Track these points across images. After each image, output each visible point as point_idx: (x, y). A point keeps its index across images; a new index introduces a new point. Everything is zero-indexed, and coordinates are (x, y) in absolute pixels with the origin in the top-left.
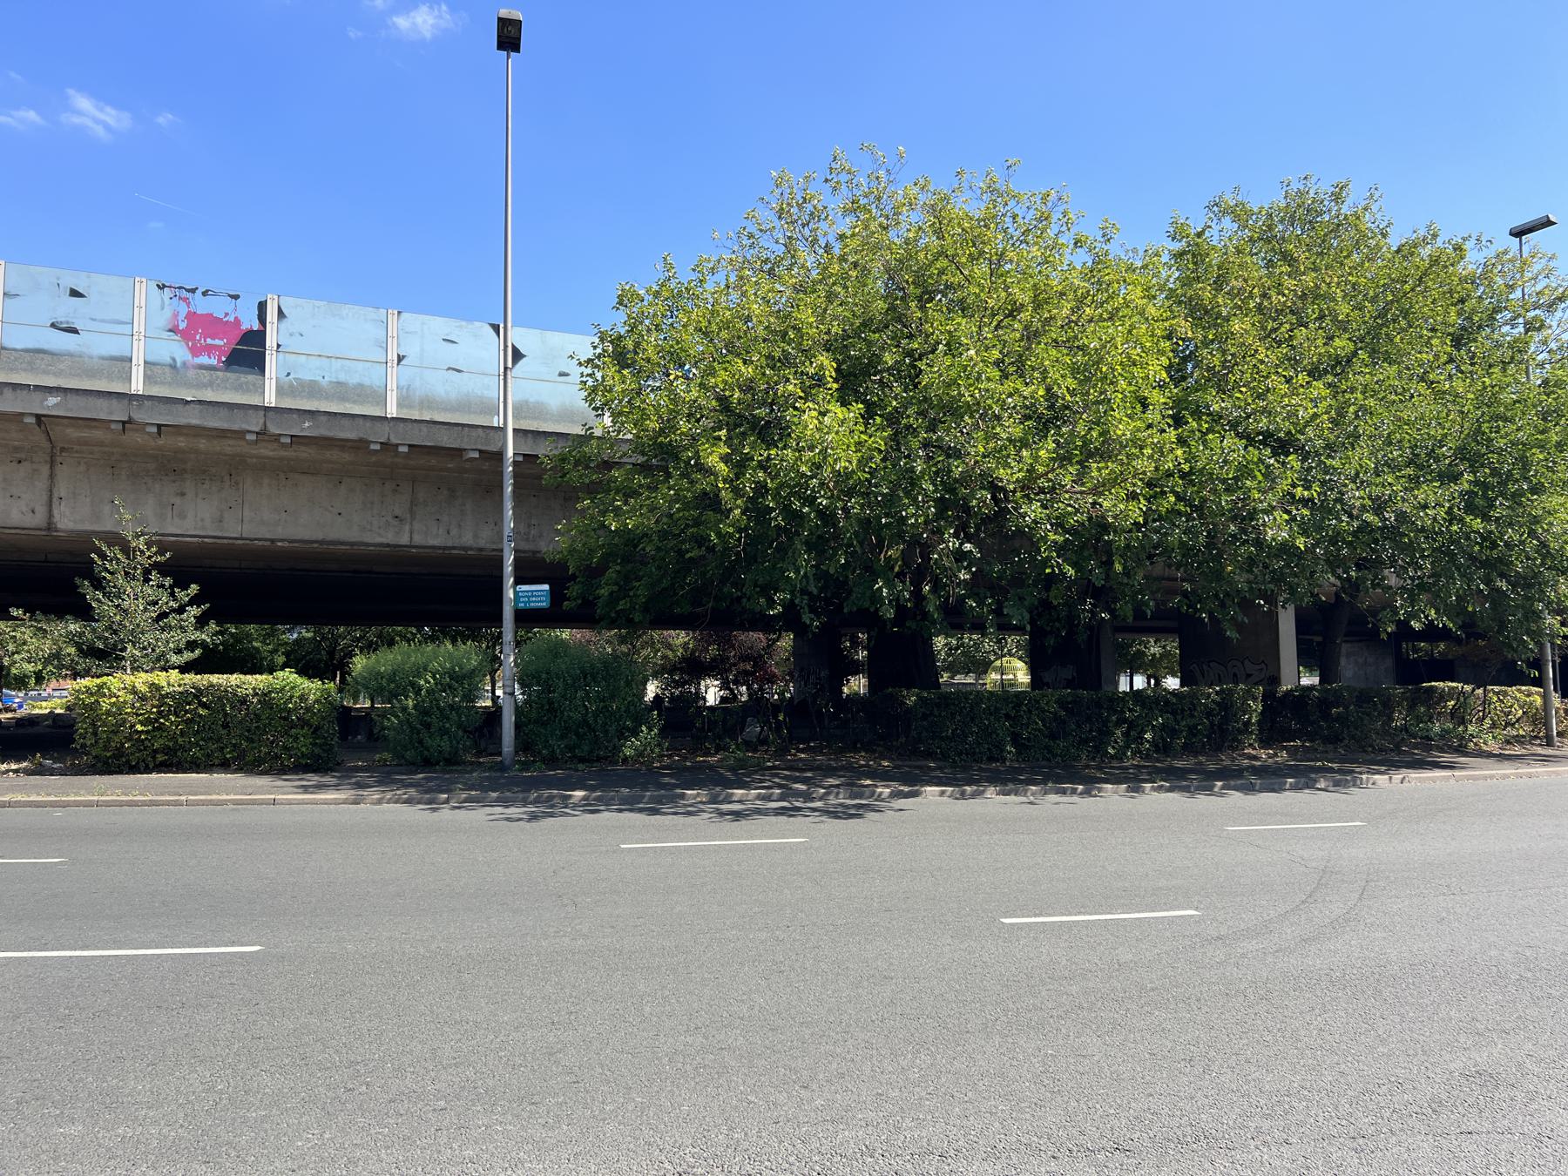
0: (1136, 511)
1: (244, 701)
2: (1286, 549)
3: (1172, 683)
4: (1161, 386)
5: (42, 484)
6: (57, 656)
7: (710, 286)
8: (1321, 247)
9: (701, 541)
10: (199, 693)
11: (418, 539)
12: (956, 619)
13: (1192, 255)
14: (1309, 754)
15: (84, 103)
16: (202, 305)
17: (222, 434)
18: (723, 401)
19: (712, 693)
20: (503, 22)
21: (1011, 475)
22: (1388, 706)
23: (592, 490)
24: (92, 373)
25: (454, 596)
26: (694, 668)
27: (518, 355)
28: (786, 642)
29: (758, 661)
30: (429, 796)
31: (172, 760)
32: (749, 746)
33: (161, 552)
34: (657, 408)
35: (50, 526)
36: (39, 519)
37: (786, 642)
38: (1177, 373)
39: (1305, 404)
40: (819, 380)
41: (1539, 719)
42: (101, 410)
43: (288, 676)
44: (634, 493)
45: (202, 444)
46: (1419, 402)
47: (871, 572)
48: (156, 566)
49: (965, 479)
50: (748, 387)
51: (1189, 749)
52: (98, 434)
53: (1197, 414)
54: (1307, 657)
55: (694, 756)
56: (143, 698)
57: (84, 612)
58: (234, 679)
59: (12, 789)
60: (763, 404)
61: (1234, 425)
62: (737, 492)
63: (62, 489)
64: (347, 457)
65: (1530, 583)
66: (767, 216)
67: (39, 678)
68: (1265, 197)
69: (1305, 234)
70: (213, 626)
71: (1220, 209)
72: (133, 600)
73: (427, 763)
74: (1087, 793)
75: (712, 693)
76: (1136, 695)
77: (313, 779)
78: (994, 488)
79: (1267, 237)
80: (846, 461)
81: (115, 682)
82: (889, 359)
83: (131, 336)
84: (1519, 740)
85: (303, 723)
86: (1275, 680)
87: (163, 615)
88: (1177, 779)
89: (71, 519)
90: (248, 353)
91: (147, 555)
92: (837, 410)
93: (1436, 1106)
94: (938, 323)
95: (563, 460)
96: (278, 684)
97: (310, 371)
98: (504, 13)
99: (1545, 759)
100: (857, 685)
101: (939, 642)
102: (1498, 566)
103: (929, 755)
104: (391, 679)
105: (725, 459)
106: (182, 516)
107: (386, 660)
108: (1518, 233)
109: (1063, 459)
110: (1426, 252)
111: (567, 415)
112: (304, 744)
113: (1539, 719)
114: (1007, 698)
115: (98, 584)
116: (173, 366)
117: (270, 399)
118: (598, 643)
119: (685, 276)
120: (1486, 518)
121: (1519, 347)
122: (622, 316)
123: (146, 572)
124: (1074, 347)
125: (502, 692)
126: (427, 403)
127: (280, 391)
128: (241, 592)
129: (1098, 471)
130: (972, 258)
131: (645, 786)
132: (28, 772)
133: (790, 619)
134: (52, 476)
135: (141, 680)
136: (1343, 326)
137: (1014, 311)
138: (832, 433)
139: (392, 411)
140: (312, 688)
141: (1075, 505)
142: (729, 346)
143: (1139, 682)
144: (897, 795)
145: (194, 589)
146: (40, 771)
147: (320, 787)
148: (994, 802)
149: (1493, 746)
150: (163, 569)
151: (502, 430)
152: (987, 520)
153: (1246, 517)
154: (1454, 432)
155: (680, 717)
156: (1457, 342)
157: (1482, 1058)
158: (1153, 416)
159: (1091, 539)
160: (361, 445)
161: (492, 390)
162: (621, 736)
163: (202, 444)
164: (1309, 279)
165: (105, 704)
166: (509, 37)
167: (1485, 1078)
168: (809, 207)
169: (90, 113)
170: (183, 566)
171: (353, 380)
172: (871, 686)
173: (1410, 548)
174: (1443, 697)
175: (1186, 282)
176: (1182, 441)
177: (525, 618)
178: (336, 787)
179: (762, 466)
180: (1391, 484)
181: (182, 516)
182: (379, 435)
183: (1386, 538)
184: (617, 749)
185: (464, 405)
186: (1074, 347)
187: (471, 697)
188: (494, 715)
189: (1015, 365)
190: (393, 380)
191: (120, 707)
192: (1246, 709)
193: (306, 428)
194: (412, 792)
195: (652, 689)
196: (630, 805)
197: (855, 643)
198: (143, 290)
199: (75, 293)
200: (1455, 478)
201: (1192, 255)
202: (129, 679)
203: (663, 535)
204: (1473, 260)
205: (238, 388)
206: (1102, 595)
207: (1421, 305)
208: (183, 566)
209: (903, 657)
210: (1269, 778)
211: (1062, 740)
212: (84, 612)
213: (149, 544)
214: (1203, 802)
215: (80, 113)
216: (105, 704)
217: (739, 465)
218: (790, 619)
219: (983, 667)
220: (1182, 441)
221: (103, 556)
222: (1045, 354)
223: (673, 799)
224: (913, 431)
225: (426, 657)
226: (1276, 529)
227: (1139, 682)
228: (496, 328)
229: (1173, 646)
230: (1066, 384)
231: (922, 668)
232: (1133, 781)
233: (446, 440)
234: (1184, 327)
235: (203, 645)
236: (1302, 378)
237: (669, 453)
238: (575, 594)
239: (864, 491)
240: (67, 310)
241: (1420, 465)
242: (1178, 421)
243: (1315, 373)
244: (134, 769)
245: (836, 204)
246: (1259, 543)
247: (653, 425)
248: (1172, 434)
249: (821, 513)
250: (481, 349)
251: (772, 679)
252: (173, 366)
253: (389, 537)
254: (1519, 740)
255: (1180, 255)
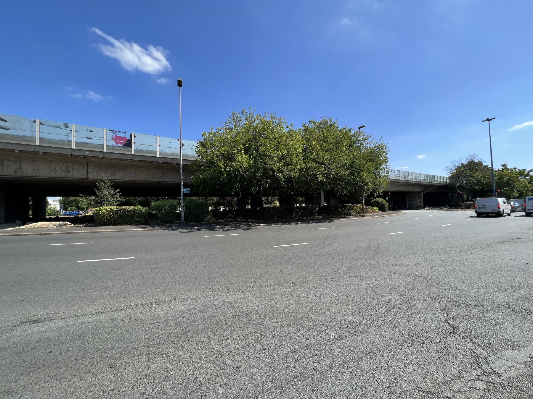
0: (297, 175)
1: (130, 211)
2: (322, 181)
3: (303, 205)
4: (301, 153)
5: (85, 170)
6: (90, 203)
7: (220, 132)
8: (327, 129)
9: (219, 180)
10: (120, 210)
11: (164, 180)
12: (266, 194)
13: (306, 130)
14: (325, 216)
15: (91, 93)
16: (118, 134)
17: (123, 160)
18: (223, 154)
19: (222, 209)
20: (179, 81)
21: (275, 168)
22: (338, 208)
23: (198, 170)
24: (96, 147)
25: (172, 191)
26: (218, 204)
27: (183, 145)
28: (235, 199)
29: (230, 202)
30: (168, 229)
31: (115, 223)
32: (229, 218)
33: (111, 183)
34: (210, 155)
35: (88, 178)
36: (85, 176)
37: (235, 199)
38: (304, 151)
39: (325, 156)
40: (241, 150)
41: (362, 210)
42: (97, 155)
43: (139, 206)
44: (206, 171)
45: (119, 162)
46: (343, 156)
47: (251, 186)
48: (110, 186)
49: (267, 169)
50: (227, 151)
51: (306, 216)
52: (97, 159)
53: (307, 158)
54: (325, 200)
55: (218, 221)
56: (109, 211)
57: (96, 195)
58: (127, 207)
59: (82, 230)
60: (230, 154)
61: (313, 160)
62: (225, 171)
63: (90, 170)
64: (149, 164)
65: (360, 187)
66: (231, 120)
67: (87, 208)
68: (318, 120)
69: (325, 127)
70: (123, 197)
71: (311, 122)
72: (106, 192)
73: (167, 222)
74: (289, 224)
75: (222, 209)
76: (297, 207)
77: (144, 226)
78: (272, 170)
79: (318, 127)
80: (246, 165)
81: (102, 208)
82: (253, 147)
83: (104, 140)
84: (359, 213)
85: (142, 215)
86: (320, 204)
87: (112, 195)
88: (303, 221)
89: (92, 176)
90: (128, 144)
91: (109, 183)
92: (244, 156)
93: (344, 273)
94: (262, 141)
95: (192, 165)
96: (136, 208)
97: (141, 147)
98: (179, 79)
99: (363, 216)
100: (249, 207)
101: (263, 199)
102: (356, 184)
103: (262, 219)
104: (159, 207)
105: (223, 165)
106: (116, 176)
107: (158, 203)
108: (359, 128)
109: (284, 165)
110: (344, 131)
111: (193, 156)
112: (142, 219)
113: (362, 210)
114: (276, 208)
115: (98, 189)
116: (113, 146)
117: (133, 153)
118: (200, 199)
119: (215, 131)
120: (354, 176)
121: (359, 147)
122: (203, 138)
123: (108, 187)
124: (286, 146)
125: (180, 209)
126: (165, 154)
127: (135, 151)
128: (128, 191)
129: (291, 168)
130: (268, 129)
131: (209, 226)
132: (84, 226)
133: (236, 195)
134: (87, 168)
135: (108, 208)
136: (331, 143)
137: (275, 139)
138: (243, 160)
139: (158, 155)
140: (143, 209)
141: (286, 173)
142: (224, 144)
143: (298, 205)
144: (256, 226)
145: (118, 190)
146: (87, 226)
147: (146, 228)
148: (273, 226)
149: (355, 214)
150: (112, 186)
151: (180, 159)
152: (271, 176)
153: (315, 176)
154: (348, 162)
155: (216, 212)
156: (350, 147)
157: (351, 265)
158: (299, 158)
159: (289, 180)
160: (152, 162)
161: (178, 151)
162: (205, 217)
163: (119, 162)
164: (326, 135)
165: (101, 213)
166: (180, 84)
167: (352, 268)
168: (238, 119)
169: (93, 96)
170: (116, 185)
171: (150, 149)
172: (251, 207)
173: (342, 182)
174: (347, 206)
175: (305, 135)
176: (304, 163)
177: (186, 195)
178: (149, 227)
179: (230, 166)
180: (339, 170)
181: (116, 176)
182: (156, 160)
183: (336, 181)
184: (204, 219)
185: (173, 154)
186: (286, 146)
187: (176, 209)
188: (180, 214)
189: (276, 148)
190: (158, 150)
191: (104, 213)
192: (315, 209)
193: (141, 158)
194: (164, 228)
195: (210, 208)
196: (206, 229)
197: (248, 199)
198: (106, 131)
199: (91, 131)
200: (349, 169)
201: (306, 130)
202: (105, 208)
203: (212, 179)
204: (352, 133)
205: (126, 151)
206: (292, 190)
207: (344, 139)
208: (116, 185)
209: (256, 202)
210: (320, 221)
211: (284, 216)
212: (96, 195)
213: (109, 181)
214: (308, 225)
215: (91, 95)
216: (101, 213)
217: (226, 166)
218: (236, 195)
219: (271, 203)
220: (304, 163)
221: (99, 184)
222: (281, 147)
223: (214, 228)
224: (258, 160)
225: (167, 202)
226: (320, 178)
227: (298, 205)
228: (178, 140)
229: (303, 199)
230: (285, 152)
231: (261, 203)
232: (297, 222)
233: (169, 161)
234: (305, 142)
235: (121, 201)
236: (325, 152)
237: (213, 164)
238: (195, 190)
239: (249, 171)
240: (90, 135)
241: (344, 167)
242: (304, 159)
243: (327, 151)
244: (107, 225)
245: (243, 118)
246: (317, 180)
247: (209, 158)
248: (303, 161)
249: (241, 175)
250: (175, 144)
251: (233, 206)
252: (113, 146)
253: (158, 180)
254: (359, 213)
255: (304, 130)
